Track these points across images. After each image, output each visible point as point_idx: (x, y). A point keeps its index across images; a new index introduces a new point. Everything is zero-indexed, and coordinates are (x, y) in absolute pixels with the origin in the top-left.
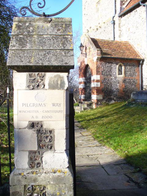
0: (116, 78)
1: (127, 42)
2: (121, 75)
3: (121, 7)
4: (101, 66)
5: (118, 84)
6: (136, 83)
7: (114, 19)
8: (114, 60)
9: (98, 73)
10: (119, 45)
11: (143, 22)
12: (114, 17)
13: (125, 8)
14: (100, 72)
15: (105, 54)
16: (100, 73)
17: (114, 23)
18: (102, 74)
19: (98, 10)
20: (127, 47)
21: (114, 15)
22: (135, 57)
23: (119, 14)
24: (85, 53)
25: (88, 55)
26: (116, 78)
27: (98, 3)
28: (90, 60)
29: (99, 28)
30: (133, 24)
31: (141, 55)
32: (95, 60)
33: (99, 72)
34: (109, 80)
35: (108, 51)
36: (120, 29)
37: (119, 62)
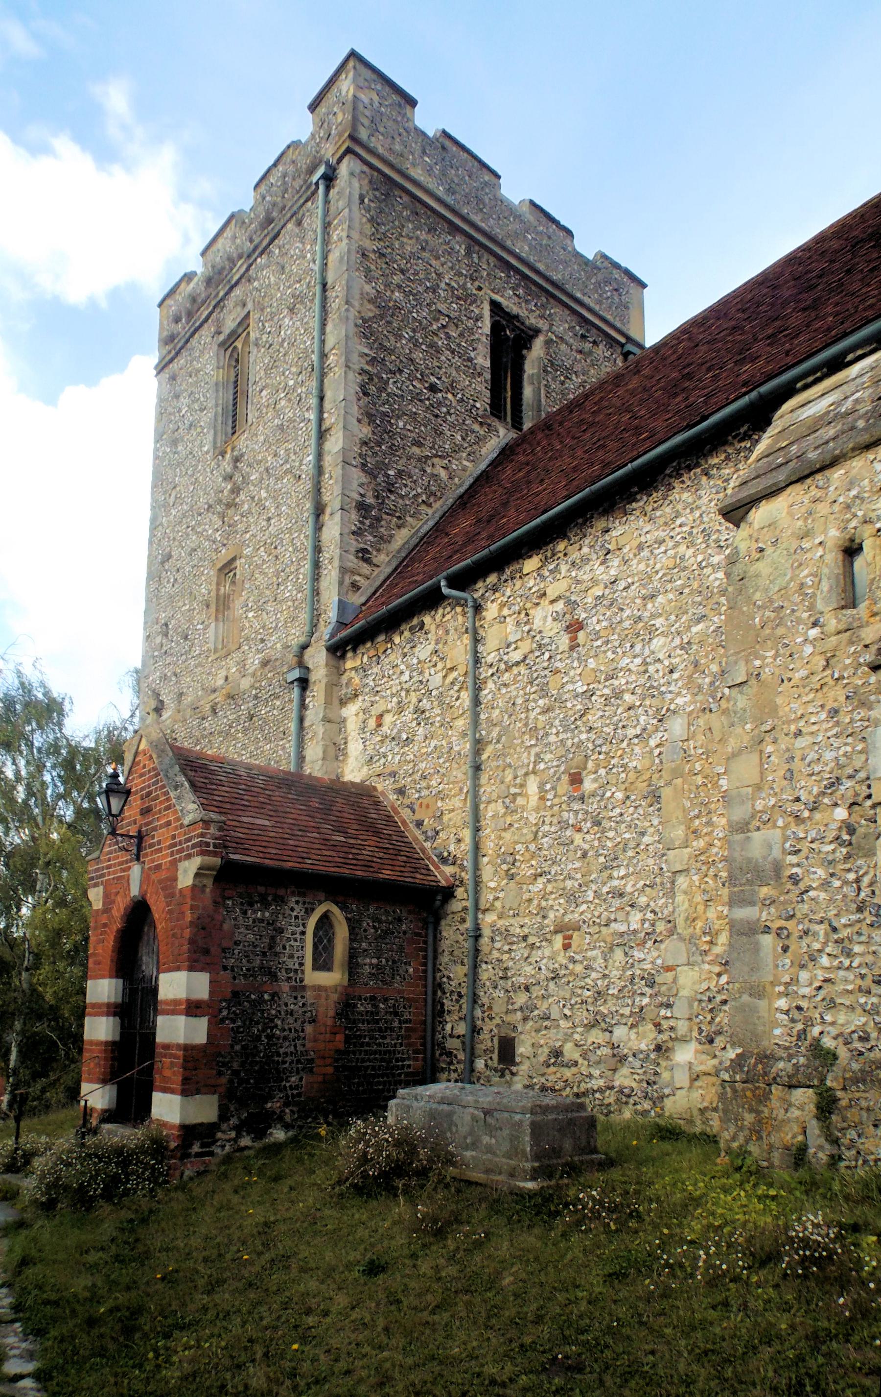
3: (340, 601)
6: (406, 1021)
11: (456, 688)
12: (304, 647)
17: (304, 683)
21: (303, 640)
32: (186, 874)
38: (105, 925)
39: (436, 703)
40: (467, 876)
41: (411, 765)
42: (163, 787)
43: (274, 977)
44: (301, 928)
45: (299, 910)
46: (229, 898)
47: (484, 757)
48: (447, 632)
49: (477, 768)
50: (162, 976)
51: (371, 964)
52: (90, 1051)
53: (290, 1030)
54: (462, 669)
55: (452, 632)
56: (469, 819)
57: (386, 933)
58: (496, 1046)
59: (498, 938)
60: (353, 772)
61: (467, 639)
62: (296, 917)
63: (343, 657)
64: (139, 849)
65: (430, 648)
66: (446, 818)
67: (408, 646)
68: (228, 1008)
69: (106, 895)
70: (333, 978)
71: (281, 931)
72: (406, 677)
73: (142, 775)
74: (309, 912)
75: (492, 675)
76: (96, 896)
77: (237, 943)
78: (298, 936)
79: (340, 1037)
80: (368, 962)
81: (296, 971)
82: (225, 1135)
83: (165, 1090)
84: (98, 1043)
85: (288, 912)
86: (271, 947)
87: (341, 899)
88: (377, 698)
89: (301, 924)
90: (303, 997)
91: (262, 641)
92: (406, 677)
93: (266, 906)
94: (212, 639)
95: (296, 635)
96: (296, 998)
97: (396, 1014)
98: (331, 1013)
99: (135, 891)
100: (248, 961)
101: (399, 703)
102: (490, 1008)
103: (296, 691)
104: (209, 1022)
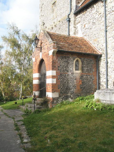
0: (73, 73)
1: (83, 38)
2: (78, 70)
3: (76, 5)
4: (57, 61)
5: (75, 81)
6: (93, 79)
7: (70, 17)
8: (71, 55)
9: (53, 68)
10: (75, 40)
11: (101, 17)
12: (69, 15)
13: (80, 6)
14: (56, 67)
15: (60, 48)
16: (55, 68)
17: (69, 21)
18: (59, 70)
19: (53, 11)
20: (83, 42)
21: (69, 13)
22: (92, 53)
23: (75, 12)
24: (40, 47)
25: (43, 49)
26: (73, 73)
27: (54, 3)
28: (45, 54)
29: (53, 26)
30: (90, 20)
31: (98, 51)
32: (51, 53)
33: (55, 67)
34: (65, 76)
35: (64, 45)
36: (75, 26)
37: (76, 57)
38: (36, 64)
39: (97, 21)
40: (105, 52)
41: (92, 33)
42: (45, 38)
43: (68, 71)
44: (73, 62)
45: (72, 59)
46: (59, 57)
47: (108, 29)
48: (99, 7)
49: (106, 31)
50: (47, 72)
51: (86, 69)
52: (34, 86)
53: (71, 81)
54: (102, 13)
55: (100, 7)
56: (105, 41)
57: (89, 63)
58: (112, 83)
59: (112, 63)
60: (79, 35)
61: (103, 7)
62: (72, 60)
63: (77, 16)
64: (41, 50)
65: (95, 10)
66: (99, 42)
67: (90, 11)
68: (60, 77)
69: (36, 59)
70: (79, 72)
71: (69, 63)
72: (90, 17)
73: (41, 37)
74: (74, 59)
75: (109, 13)
76: (34, 59)
77: (61, 65)
78: (72, 64)
79: (81, 82)
80: (85, 69)
81: (72, 70)
82: (60, 100)
83: (49, 92)
84: (36, 84)
85: (70, 60)
86: (67, 66)
87: (80, 57)
88: (84, 22)
89: (73, 62)
90: (73, 75)
91: (61, 15)
92: (90, 17)
93: (66, 58)
94: (51, 17)
95: (68, 12)
96: (72, 75)
97: (91, 78)
98: (79, 78)
99: (41, 57)
100: (63, 68)
101: (89, 22)
102: (111, 76)
103: (68, 22)
104: (56, 80)
